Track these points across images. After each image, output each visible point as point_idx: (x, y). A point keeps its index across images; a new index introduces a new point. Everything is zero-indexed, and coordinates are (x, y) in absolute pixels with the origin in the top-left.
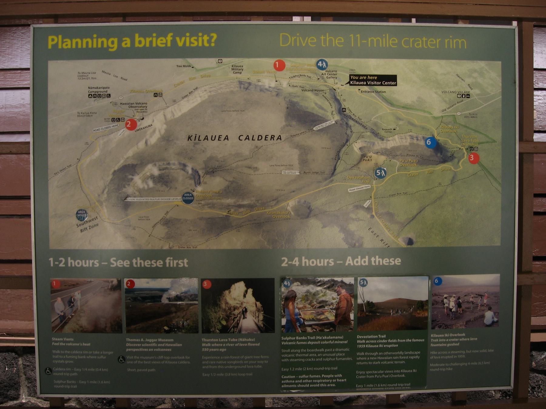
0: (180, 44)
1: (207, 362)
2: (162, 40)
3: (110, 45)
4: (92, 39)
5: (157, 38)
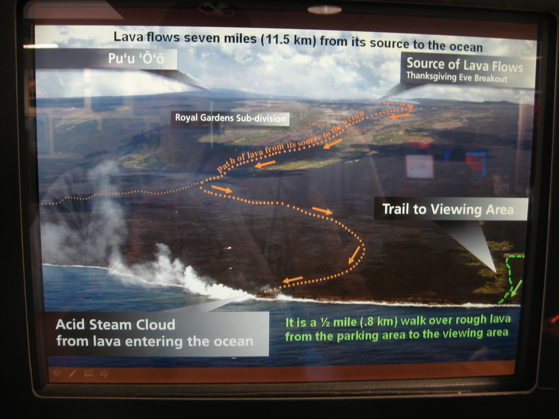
2: (447, 209)
3: (476, 212)
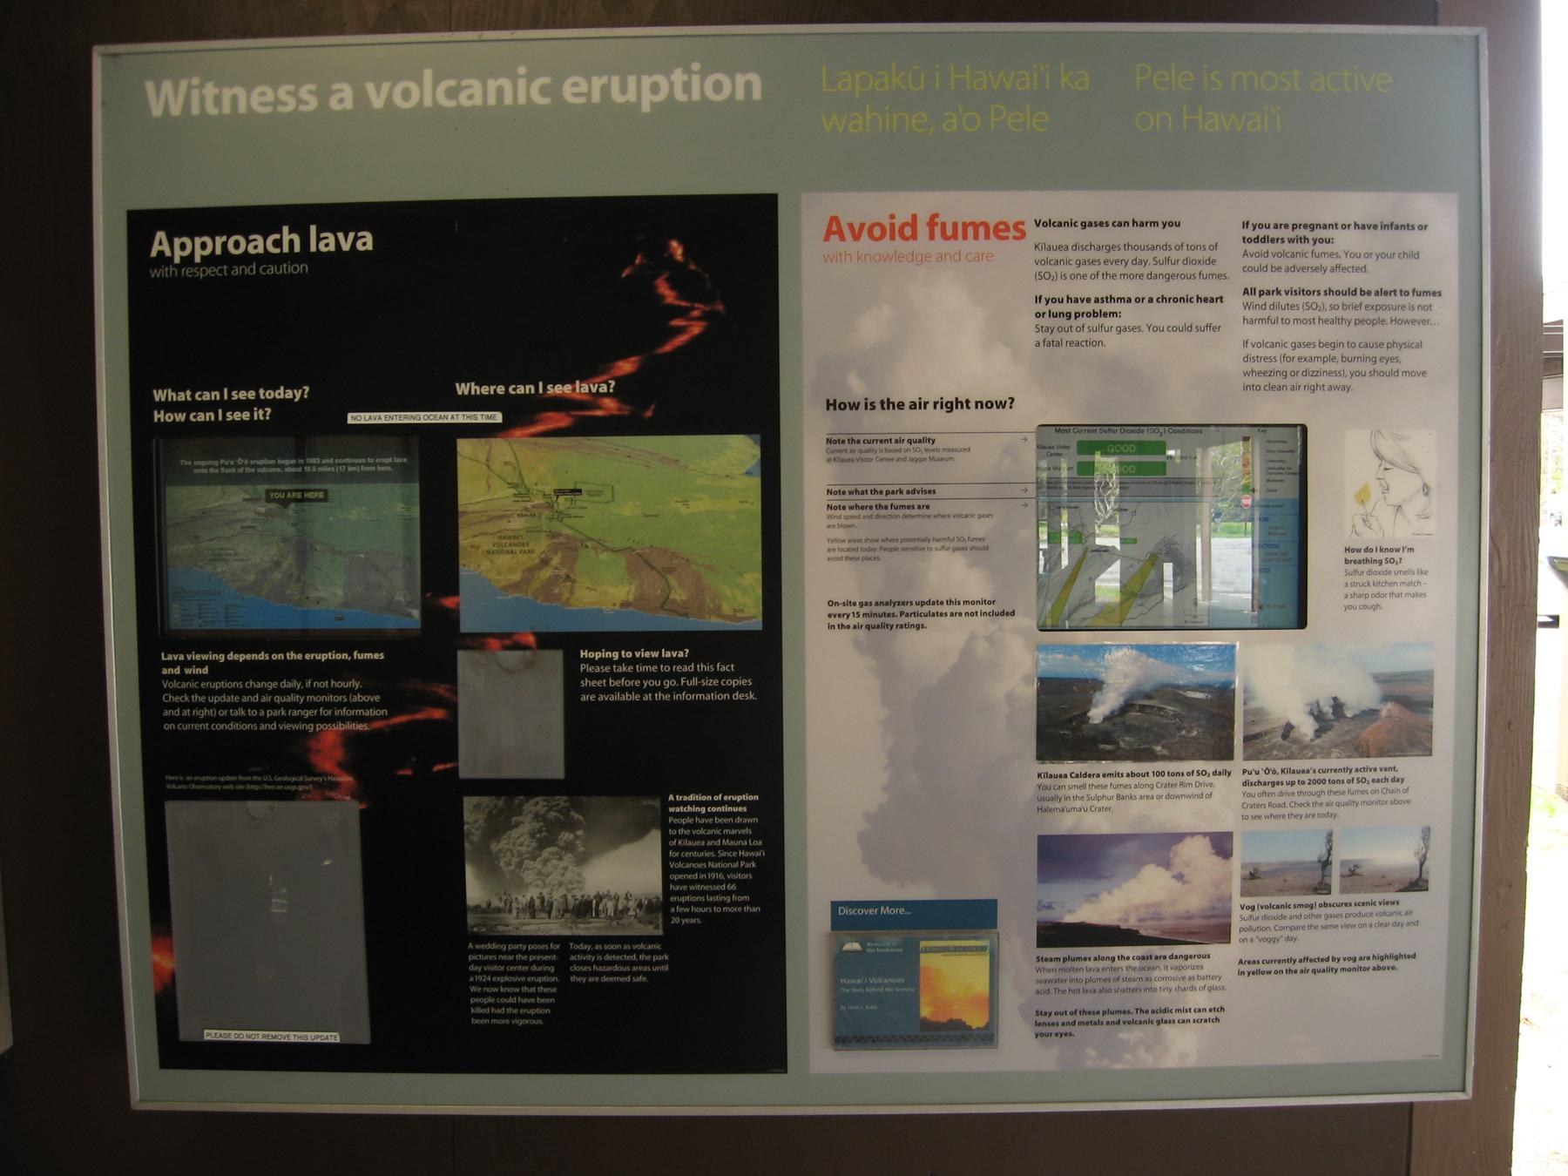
0: (378, 103)
1: (176, 713)
2: (576, 84)
4: (514, 78)
5: (704, 74)
